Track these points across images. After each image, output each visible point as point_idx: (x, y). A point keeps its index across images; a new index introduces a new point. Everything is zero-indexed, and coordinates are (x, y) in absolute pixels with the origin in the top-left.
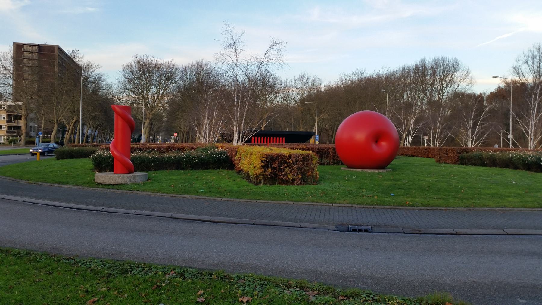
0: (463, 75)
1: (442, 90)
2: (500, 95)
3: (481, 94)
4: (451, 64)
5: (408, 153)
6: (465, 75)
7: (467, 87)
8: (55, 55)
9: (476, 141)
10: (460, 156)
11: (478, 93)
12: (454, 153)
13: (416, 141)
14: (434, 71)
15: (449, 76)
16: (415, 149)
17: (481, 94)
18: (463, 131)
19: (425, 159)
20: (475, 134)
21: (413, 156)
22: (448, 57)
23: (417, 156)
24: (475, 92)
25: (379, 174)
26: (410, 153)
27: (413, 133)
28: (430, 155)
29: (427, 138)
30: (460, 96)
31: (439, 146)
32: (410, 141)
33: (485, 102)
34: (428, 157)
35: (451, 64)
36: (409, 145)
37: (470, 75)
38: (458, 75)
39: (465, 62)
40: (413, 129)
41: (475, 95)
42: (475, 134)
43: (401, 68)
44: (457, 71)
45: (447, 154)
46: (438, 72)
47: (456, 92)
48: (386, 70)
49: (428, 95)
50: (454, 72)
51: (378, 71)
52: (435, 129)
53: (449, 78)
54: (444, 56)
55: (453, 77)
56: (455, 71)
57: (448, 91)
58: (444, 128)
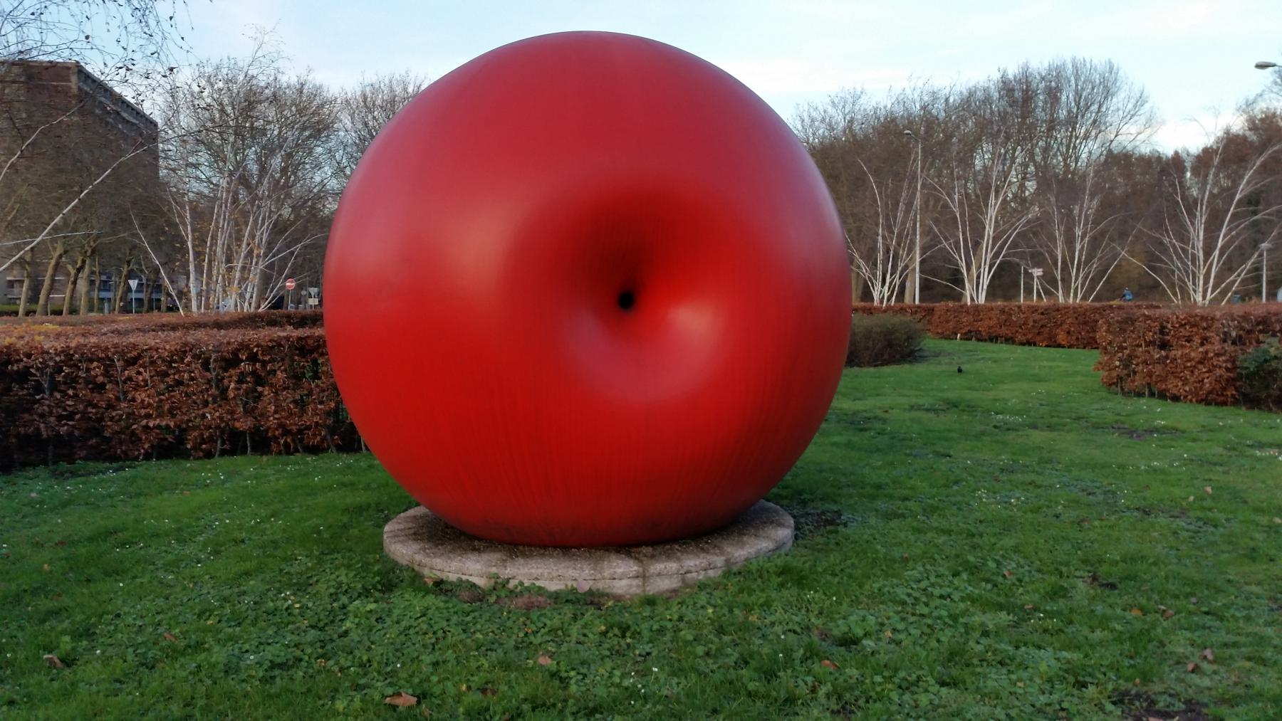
0: (1130, 106)
1: (1075, 147)
2: (1231, 153)
3: (1176, 153)
4: (1097, 78)
5: (984, 330)
6: (1135, 106)
7: (1140, 137)
8: (70, 88)
9: (1220, 278)
10: (1249, 357)
11: (1170, 153)
12: (1205, 340)
13: (1005, 280)
14: (1053, 95)
15: (1094, 108)
16: (1003, 311)
17: (1176, 153)
18: (1169, 240)
19: (1041, 352)
20: (1217, 253)
21: (993, 339)
22: (1088, 60)
23: (1009, 340)
24: (1160, 150)
25: (691, 590)
26: (983, 327)
27: (996, 256)
28: (1061, 337)
29: (1037, 272)
30: (1121, 161)
31: (1084, 298)
32: (985, 281)
33: (1188, 174)
34: (1054, 344)
35: (1097, 78)
36: (982, 300)
37: (1147, 106)
38: (1117, 103)
39: (1135, 76)
40: (995, 239)
41: (1159, 158)
42: (1217, 253)
43: (965, 93)
44: (1112, 95)
45: (1164, 345)
46: (1064, 98)
47: (1110, 151)
48: (920, 84)
49: (1038, 158)
50: (1106, 98)
51: (899, 91)
52: (1070, 242)
53: (1090, 116)
54: (1079, 57)
55: (1103, 109)
56: (1108, 93)
57: (1090, 151)
58: (1103, 234)
